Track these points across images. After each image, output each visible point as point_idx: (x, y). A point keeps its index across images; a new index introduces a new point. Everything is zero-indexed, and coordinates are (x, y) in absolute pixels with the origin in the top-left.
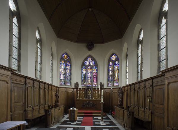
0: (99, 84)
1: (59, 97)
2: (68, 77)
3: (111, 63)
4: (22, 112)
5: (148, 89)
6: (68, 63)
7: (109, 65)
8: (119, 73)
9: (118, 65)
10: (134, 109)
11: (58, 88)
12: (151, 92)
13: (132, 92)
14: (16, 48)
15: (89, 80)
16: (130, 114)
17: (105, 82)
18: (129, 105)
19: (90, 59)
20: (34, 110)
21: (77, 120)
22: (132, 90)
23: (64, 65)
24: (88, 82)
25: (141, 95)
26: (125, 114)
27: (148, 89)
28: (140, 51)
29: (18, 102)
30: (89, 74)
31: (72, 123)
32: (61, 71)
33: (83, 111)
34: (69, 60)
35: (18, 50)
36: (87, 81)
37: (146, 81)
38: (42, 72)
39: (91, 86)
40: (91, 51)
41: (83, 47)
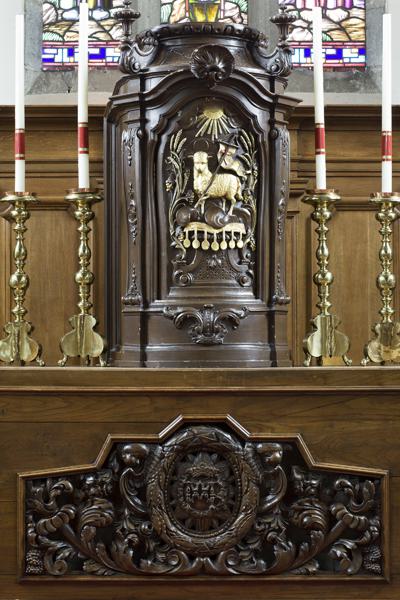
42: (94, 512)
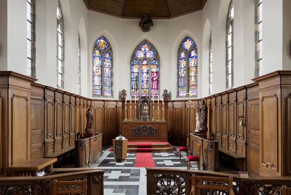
0: (162, 92)
1: (94, 118)
2: (106, 81)
3: (183, 55)
4: (40, 144)
5: (241, 105)
6: (107, 56)
7: (179, 58)
8: (196, 72)
9: (196, 57)
10: (222, 138)
11: (89, 102)
12: (245, 110)
13: (218, 109)
14: (29, 39)
15: (145, 85)
16: (212, 147)
17: (172, 90)
18: (214, 132)
19: (145, 48)
20: (56, 143)
21: (127, 158)
22: (218, 104)
23: (100, 59)
24: (142, 89)
25: (232, 115)
26: (205, 146)
27: (241, 105)
28: (230, 37)
29: (35, 129)
30: (145, 74)
31: (118, 164)
32: (94, 69)
33: (136, 143)
34: (109, 50)
35: (32, 43)
36: (140, 86)
37: (239, 90)
38: (65, 75)
39: (148, 97)
40: (147, 32)
41: (132, 26)
42: (137, 131)
